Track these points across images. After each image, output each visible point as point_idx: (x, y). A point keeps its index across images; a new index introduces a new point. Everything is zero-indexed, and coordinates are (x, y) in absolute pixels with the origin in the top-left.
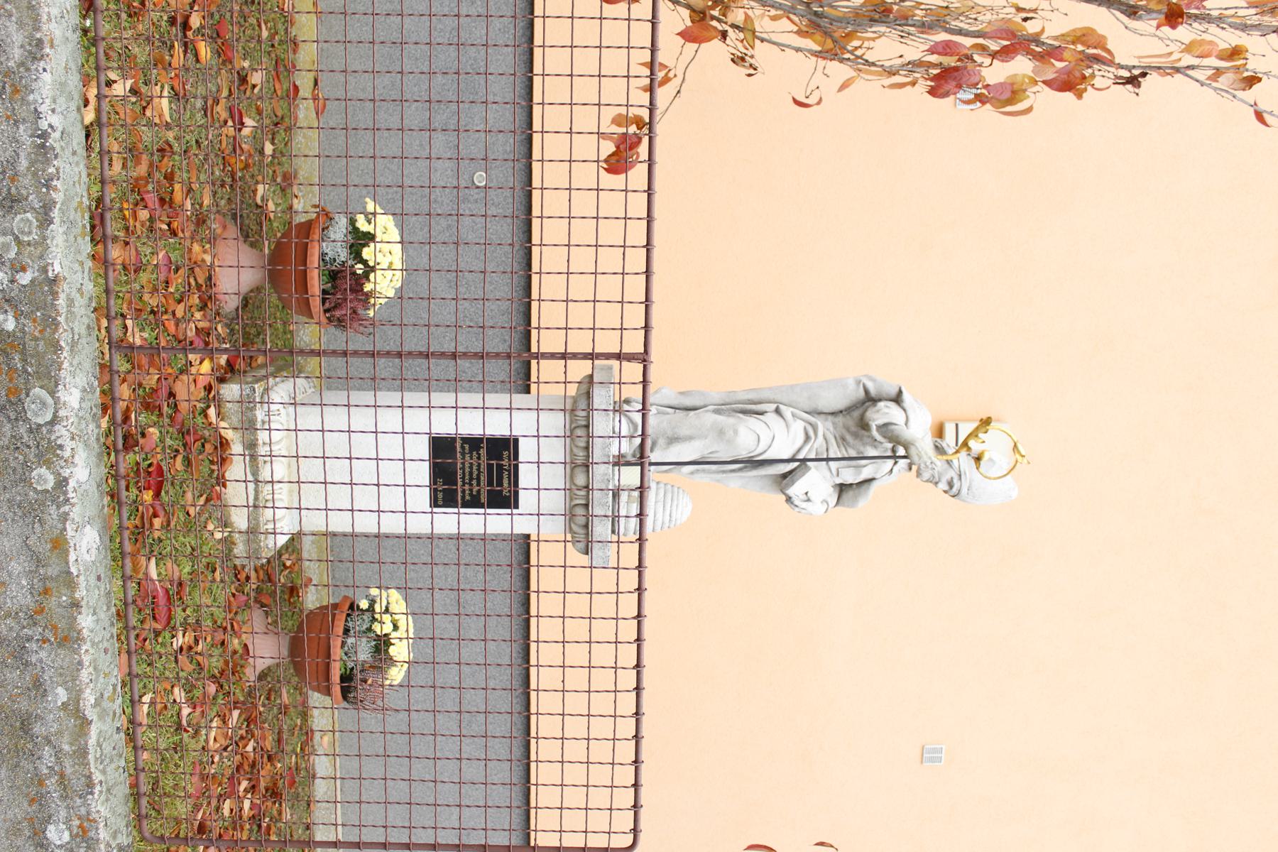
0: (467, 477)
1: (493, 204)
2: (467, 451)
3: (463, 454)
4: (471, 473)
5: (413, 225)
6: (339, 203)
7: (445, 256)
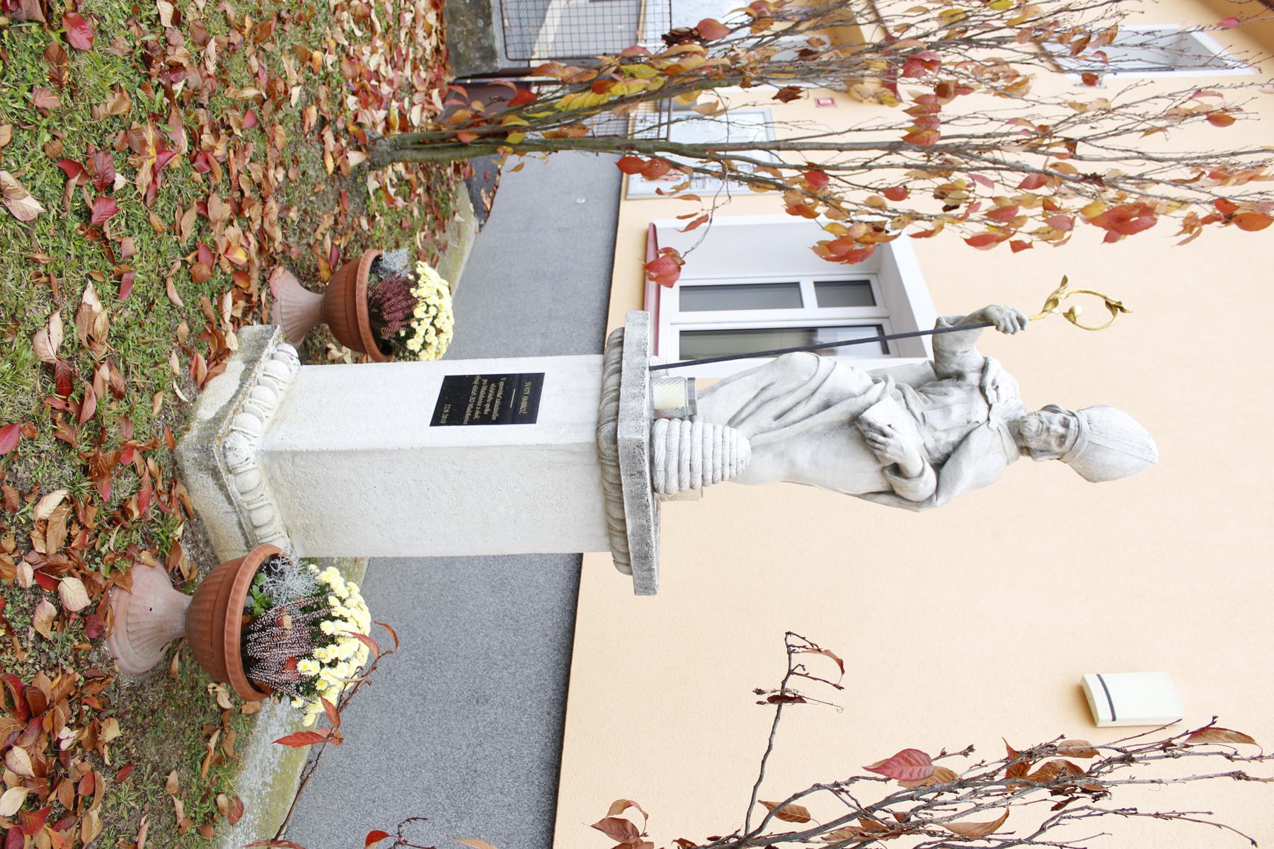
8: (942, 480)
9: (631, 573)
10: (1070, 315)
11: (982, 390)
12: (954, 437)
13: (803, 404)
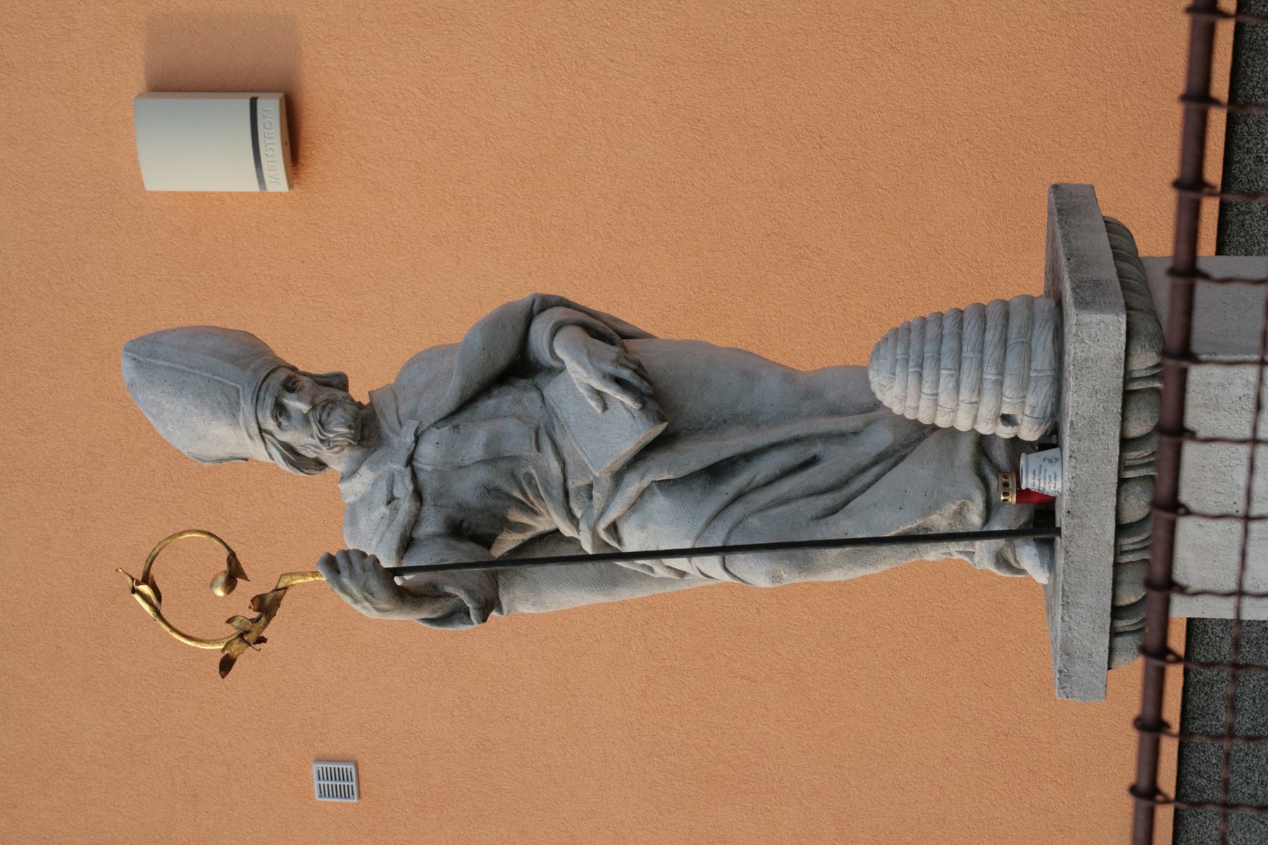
8: (520, 328)
9: (1103, 217)
10: (234, 574)
11: (418, 494)
12: (488, 405)
13: (760, 478)
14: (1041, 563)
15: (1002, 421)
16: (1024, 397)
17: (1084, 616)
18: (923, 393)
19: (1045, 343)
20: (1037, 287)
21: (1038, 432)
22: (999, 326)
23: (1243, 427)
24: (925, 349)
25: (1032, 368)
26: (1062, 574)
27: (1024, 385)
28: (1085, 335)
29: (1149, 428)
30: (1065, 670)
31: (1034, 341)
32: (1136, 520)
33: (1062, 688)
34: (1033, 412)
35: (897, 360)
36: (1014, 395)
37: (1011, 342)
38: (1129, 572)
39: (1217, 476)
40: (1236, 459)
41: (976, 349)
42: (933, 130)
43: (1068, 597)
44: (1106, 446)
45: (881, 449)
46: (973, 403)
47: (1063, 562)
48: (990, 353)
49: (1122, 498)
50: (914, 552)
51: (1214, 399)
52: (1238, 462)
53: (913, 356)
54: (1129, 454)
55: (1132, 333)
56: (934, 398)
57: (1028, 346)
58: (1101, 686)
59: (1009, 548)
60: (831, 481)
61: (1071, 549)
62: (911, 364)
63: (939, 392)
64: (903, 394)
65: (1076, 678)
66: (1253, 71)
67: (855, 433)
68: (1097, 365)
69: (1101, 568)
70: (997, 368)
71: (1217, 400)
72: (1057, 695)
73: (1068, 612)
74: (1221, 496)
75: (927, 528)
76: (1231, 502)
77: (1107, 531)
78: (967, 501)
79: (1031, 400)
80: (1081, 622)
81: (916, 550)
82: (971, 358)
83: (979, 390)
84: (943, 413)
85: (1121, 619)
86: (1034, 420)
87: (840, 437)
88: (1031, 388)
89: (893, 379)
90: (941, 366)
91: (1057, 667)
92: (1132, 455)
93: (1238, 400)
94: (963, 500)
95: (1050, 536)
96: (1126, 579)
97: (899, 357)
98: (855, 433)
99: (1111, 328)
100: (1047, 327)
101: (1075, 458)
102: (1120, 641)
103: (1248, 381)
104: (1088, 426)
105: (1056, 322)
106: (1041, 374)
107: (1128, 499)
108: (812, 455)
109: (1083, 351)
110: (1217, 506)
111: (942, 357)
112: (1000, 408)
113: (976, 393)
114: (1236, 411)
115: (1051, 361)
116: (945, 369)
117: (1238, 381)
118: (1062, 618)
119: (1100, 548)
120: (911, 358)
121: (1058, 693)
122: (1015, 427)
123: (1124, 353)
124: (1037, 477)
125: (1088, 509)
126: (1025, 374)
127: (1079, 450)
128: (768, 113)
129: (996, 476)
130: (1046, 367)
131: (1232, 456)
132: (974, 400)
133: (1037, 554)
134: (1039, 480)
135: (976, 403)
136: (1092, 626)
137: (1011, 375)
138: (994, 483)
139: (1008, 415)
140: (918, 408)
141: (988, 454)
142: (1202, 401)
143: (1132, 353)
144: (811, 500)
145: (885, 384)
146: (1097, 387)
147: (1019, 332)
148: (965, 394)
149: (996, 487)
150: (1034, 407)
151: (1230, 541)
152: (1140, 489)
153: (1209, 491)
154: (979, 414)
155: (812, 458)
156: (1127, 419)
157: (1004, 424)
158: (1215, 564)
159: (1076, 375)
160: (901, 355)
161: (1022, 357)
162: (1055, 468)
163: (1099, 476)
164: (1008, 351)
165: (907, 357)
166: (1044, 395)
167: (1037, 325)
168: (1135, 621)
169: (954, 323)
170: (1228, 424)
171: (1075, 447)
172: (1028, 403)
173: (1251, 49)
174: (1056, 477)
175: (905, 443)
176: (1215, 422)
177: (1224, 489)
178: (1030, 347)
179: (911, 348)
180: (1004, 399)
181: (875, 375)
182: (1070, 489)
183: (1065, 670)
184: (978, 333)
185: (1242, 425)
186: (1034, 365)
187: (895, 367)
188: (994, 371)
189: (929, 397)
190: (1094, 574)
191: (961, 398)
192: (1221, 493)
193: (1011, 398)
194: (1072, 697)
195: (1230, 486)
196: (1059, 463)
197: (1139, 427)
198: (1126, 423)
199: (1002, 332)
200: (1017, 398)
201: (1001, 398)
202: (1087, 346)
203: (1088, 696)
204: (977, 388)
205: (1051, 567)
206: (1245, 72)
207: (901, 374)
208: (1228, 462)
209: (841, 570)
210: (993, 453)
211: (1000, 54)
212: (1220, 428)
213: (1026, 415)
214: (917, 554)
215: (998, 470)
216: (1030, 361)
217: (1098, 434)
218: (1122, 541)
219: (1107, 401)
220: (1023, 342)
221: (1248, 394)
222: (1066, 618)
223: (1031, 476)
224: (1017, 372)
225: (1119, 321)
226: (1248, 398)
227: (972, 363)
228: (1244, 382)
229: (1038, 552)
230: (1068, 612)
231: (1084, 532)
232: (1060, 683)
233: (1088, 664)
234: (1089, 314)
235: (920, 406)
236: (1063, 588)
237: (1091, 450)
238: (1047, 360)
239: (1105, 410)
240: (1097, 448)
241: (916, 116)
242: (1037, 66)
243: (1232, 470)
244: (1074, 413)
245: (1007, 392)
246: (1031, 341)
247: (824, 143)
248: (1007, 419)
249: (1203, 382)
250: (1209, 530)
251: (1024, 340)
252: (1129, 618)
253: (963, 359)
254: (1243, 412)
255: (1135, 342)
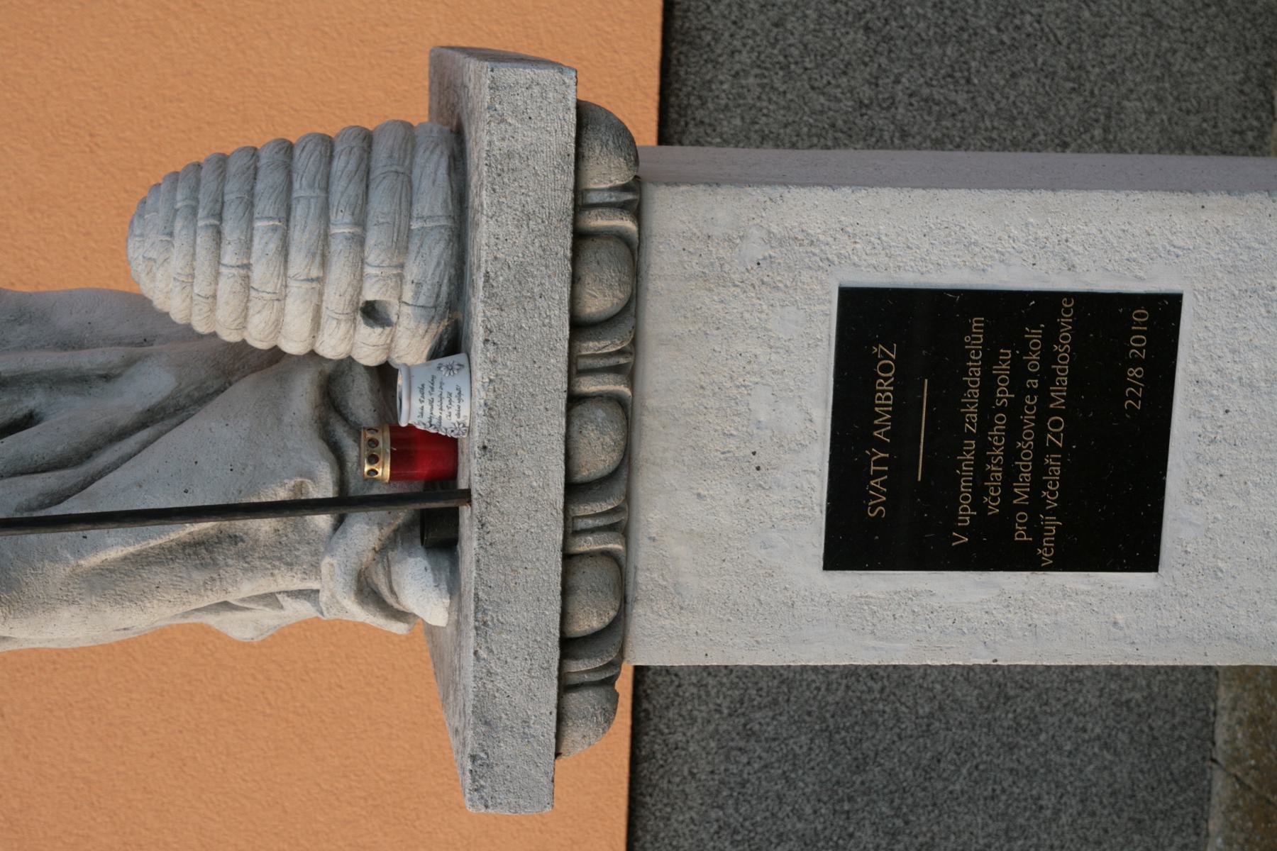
0: (1029, 416)
1: (736, 832)
2: (1022, 517)
3: (1036, 505)
4: (1014, 431)
5: (958, 770)
6: (1159, 823)
7: (877, 687)
14: (435, 581)
15: (364, 318)
16: (402, 266)
17: (514, 647)
18: (224, 265)
19: (436, 173)
20: (418, 111)
21: (427, 338)
22: (355, 149)
23: (763, 316)
24: (228, 188)
25: (415, 214)
26: (474, 568)
27: (402, 243)
28: (505, 109)
29: (616, 301)
30: (482, 755)
31: (417, 172)
32: (599, 475)
33: (476, 790)
34: (416, 295)
35: (177, 210)
36: (383, 261)
37: (377, 173)
38: (588, 571)
39: (724, 405)
40: (755, 373)
41: (317, 185)
42: (258, 130)
43: (485, 612)
44: (547, 321)
45: (153, 401)
46: (312, 280)
47: (475, 544)
48: (340, 189)
49: (575, 429)
50: (213, 580)
51: (717, 264)
52: (758, 380)
53: (205, 199)
54: (585, 345)
55: (585, 120)
56: (243, 272)
57: (406, 179)
58: (544, 780)
59: (380, 565)
60: (59, 449)
61: (490, 519)
62: (201, 213)
63: (251, 262)
64: (187, 270)
65: (501, 767)
66: (687, 73)
67: (107, 377)
68: (528, 165)
69: (542, 554)
70: (353, 214)
71: (722, 266)
72: (468, 804)
73: (487, 642)
74: (732, 441)
75: (236, 536)
76: (748, 452)
77: (551, 483)
78: (306, 480)
79: (413, 271)
80: (509, 660)
81: (215, 576)
82: (308, 199)
83: (323, 256)
84: (260, 304)
85: (576, 658)
86: (419, 311)
87: (81, 381)
88: (413, 248)
89: (170, 243)
90: (256, 215)
91: (468, 750)
92: (590, 346)
93: (756, 266)
94: (299, 480)
95: (451, 504)
96: (583, 583)
97: (179, 205)
98: (107, 377)
99: (551, 95)
100: (438, 151)
101: (494, 344)
102: (574, 699)
103: (769, 232)
104: (516, 282)
105: (453, 150)
106: (429, 224)
107: (584, 432)
108: (25, 411)
109: (503, 139)
110: (726, 459)
111: (256, 201)
112: (359, 291)
113: (318, 258)
114: (753, 286)
115: (445, 201)
116: (261, 219)
117: (754, 231)
118: (476, 653)
119: (539, 515)
120: (202, 203)
121: (471, 800)
122: (388, 329)
123: (573, 145)
124: (427, 397)
125: (517, 440)
126: (403, 224)
127: (500, 327)
128: (8, 95)
129: (355, 441)
130: (439, 211)
131: (748, 368)
132: (315, 273)
133: (429, 567)
134: (431, 402)
135: (318, 279)
136: (528, 666)
137: (378, 224)
138: (352, 452)
139: (375, 301)
140: (214, 296)
141: (342, 408)
142: (698, 269)
143: (586, 154)
144: (21, 480)
145: (155, 256)
146: (530, 208)
147: (391, 156)
148: (299, 263)
149: (355, 459)
150: (419, 285)
151: (747, 522)
152: (604, 415)
153: (712, 432)
154: (324, 305)
155: (25, 416)
156: (579, 279)
157: (367, 324)
158: (724, 565)
159: (492, 184)
160: (184, 200)
161: (397, 196)
162: (460, 379)
163: (535, 376)
164: (372, 186)
165: (193, 203)
166: (435, 260)
167: (421, 150)
168: (598, 663)
169: (277, 149)
170: (740, 310)
171: (494, 322)
172: (408, 278)
173: (683, 42)
174: (460, 393)
175: (196, 394)
176: (719, 307)
177: (737, 429)
178: (410, 181)
179: (202, 191)
180: (368, 270)
181: (138, 244)
182: (485, 404)
183: (482, 755)
184: (320, 160)
185: (762, 312)
186: (417, 209)
187: (173, 222)
188: (348, 219)
189: (234, 271)
190: (530, 566)
191: (291, 272)
192: (731, 435)
193: (379, 266)
194: (495, 806)
195: (745, 422)
196: (465, 371)
197: (600, 296)
198: (578, 288)
199: (361, 159)
200: (390, 266)
201: (362, 268)
202: (509, 129)
203: (521, 802)
204: (319, 252)
205: (453, 588)
206: (677, 73)
207: (184, 232)
208: (741, 380)
209: (74, 609)
210: (350, 404)
211: (351, 23)
212: (728, 317)
213: (406, 303)
214: (218, 583)
215: (356, 430)
216: (411, 204)
217: (533, 298)
218: (576, 509)
219: (546, 235)
220: (397, 172)
221: (771, 257)
222: (483, 654)
223: (416, 396)
224: (389, 220)
225: (564, 83)
226: (771, 262)
227: (309, 208)
228: (764, 234)
229: (430, 563)
230: (487, 642)
231: (513, 485)
232: (474, 781)
233: (523, 738)
234: (512, 67)
235: (219, 294)
236: (476, 595)
237: (521, 328)
238: (440, 199)
239: (544, 250)
240: (531, 323)
241: (232, 109)
242: (402, 43)
243: (749, 394)
244: (491, 258)
245: (373, 256)
246: (411, 173)
247: (97, 145)
248: (372, 313)
249: (699, 234)
250: (714, 504)
251: (400, 169)
252: (589, 657)
253: (294, 202)
254: (763, 288)
255: (591, 134)
